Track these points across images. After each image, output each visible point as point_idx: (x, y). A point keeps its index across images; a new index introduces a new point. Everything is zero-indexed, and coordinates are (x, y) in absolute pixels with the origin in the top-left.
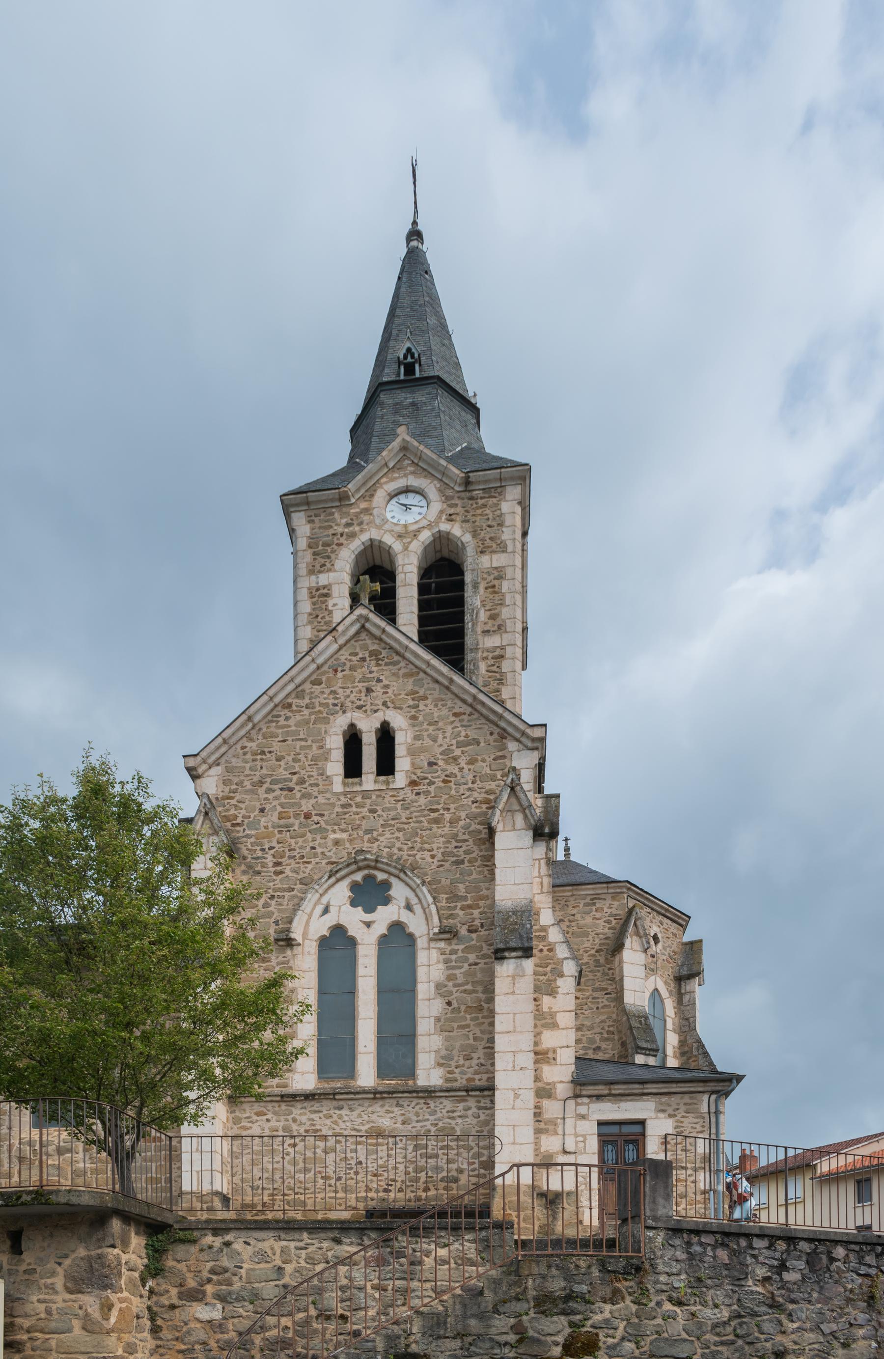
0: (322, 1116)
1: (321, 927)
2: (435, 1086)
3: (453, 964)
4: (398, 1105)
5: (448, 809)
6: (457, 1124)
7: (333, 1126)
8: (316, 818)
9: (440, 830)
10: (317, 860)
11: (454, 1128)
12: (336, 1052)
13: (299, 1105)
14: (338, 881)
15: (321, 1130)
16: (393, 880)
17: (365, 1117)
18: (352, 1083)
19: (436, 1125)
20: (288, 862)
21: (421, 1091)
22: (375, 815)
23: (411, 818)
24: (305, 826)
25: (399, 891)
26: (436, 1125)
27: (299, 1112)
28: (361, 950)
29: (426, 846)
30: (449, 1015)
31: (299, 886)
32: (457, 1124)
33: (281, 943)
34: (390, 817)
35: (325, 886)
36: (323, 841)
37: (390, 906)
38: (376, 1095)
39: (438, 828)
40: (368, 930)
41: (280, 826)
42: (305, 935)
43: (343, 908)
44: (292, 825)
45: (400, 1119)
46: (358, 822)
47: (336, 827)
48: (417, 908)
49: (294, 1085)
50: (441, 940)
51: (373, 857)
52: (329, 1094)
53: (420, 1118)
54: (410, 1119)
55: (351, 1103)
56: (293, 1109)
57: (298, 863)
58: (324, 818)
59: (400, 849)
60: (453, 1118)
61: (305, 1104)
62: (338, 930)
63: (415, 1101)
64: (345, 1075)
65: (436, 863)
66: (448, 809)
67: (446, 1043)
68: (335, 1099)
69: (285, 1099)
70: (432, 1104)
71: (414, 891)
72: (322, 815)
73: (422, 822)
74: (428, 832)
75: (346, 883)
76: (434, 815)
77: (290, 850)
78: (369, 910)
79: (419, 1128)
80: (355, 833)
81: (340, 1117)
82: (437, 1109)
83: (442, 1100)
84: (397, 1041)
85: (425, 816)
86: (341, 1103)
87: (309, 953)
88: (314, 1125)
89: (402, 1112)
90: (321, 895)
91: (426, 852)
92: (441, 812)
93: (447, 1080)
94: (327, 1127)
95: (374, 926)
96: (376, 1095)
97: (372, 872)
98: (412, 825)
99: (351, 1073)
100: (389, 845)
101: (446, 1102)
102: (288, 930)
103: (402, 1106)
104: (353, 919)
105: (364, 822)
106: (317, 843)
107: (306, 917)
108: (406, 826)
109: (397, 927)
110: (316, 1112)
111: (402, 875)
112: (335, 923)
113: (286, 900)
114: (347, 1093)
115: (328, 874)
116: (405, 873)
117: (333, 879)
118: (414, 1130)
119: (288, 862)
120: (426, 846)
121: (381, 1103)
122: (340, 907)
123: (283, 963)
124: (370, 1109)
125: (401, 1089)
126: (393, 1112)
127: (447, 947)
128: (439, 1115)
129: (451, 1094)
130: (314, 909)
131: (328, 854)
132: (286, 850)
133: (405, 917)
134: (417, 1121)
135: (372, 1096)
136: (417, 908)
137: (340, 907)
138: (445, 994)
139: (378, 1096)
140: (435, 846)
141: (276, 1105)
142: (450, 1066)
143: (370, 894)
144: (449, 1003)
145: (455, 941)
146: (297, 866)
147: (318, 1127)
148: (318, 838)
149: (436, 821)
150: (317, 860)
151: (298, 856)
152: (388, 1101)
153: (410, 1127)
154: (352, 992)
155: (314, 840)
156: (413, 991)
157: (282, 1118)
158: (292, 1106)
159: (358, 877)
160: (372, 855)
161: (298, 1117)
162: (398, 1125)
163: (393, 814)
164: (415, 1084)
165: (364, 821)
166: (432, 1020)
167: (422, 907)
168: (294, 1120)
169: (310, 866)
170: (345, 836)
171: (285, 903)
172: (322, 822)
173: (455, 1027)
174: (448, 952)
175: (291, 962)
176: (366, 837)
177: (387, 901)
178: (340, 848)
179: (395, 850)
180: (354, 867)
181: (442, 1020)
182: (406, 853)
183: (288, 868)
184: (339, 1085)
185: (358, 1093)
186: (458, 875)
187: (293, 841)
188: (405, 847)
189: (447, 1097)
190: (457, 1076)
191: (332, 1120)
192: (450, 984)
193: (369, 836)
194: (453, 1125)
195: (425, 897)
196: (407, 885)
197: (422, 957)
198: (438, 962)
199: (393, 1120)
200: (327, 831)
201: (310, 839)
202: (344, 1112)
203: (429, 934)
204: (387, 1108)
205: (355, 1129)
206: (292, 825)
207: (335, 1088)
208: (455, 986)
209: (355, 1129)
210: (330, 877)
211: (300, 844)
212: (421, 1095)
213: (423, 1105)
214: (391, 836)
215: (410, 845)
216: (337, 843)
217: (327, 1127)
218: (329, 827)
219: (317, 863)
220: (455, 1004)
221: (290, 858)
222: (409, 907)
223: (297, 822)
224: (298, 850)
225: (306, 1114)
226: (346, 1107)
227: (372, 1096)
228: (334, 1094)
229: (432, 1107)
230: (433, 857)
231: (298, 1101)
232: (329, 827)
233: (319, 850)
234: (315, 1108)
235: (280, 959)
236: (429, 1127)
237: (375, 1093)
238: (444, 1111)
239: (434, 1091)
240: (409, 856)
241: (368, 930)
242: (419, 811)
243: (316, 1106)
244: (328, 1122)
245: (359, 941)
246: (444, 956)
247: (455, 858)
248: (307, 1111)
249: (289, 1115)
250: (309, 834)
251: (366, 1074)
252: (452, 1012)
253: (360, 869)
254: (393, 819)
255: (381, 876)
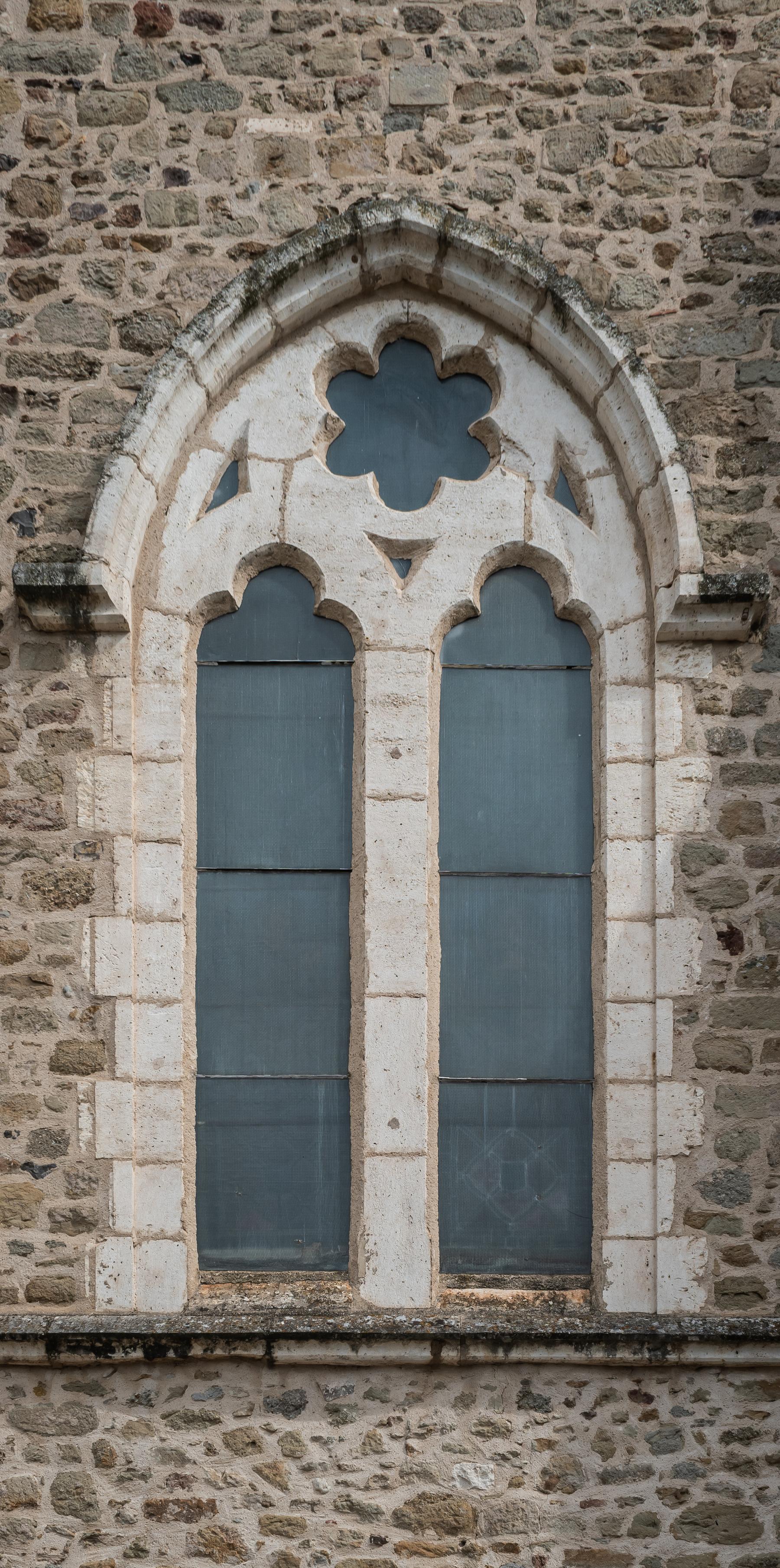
0: (218, 1443)
1: (208, 555)
2: (676, 1318)
3: (748, 757)
4: (528, 1400)
5: (729, 37)
6: (761, 1495)
7: (264, 1487)
8: (185, 35)
9: (693, 133)
10: (194, 235)
11: (748, 1513)
12: (275, 1163)
13: (122, 1387)
14: (285, 336)
15: (212, 1506)
16: (505, 357)
17: (395, 1452)
18: (340, 1292)
19: (680, 1496)
20: (73, 232)
21: (628, 1340)
22: (433, 40)
23: (578, 68)
24: (144, 69)
25: (527, 409)
26: (680, 1496)
27: (122, 1418)
28: (377, 674)
29: (639, 203)
30: (731, 992)
31: (115, 356)
32: (761, 1495)
33: (46, 614)
34: (493, 54)
35: (230, 353)
36: (216, 145)
37: (493, 475)
38: (442, 1353)
39: (688, 121)
40: (407, 576)
41: (34, 61)
42: (145, 583)
43: (303, 473)
44: (87, 62)
45: (537, 1463)
46: (362, 68)
47: (271, 85)
48: (603, 495)
49: (102, 1293)
50: (699, 642)
51: (430, 222)
52: (249, 1338)
53: (617, 1462)
54: (577, 1466)
55: (335, 1382)
56: (96, 1402)
57: (114, 243)
58: (225, 38)
59: (533, 212)
60: (746, 1467)
61: (149, 1384)
62: (282, 567)
63: (597, 1384)
64: (310, 1254)
65: (681, 289)
66: (729, 37)
67: (718, 1124)
68: (271, 1363)
69: (65, 1357)
70: (664, 1404)
71: (588, 408)
72: (213, 23)
73: (621, 88)
74: (646, 137)
75: (308, 359)
76: (671, 61)
77: (79, 179)
78: (407, 493)
79: (611, 1509)
80: (349, 117)
81: (292, 1447)
82: (685, 1422)
83: (706, 1382)
84: (526, 1130)
85: (633, 63)
86: (297, 1382)
87: (160, 672)
88: (183, 1482)
89: (545, 1432)
90: (213, 402)
91: (638, 234)
92: (700, 47)
93: (725, 1292)
94: (238, 1495)
95: (429, 565)
96: (442, 1353)
97: (418, 309)
98: (582, 98)
99: (336, 1247)
100: (488, 184)
101: (719, 1392)
102: (75, 556)
103: (543, 1405)
104: (339, 522)
105: (385, 70)
106: (190, 151)
107: (146, 503)
108: (557, 105)
109: (520, 566)
110: (191, 1420)
111: (545, 326)
112: (266, 540)
113: (63, 415)
114: (323, 1338)
115: (239, 289)
116: (561, 311)
117: (259, 326)
118: (592, 1514)
119: (73, 232)
120: (639, 203)
121: (457, 1387)
122: (288, 465)
123: (51, 716)
124: (414, 1416)
125: (544, 1325)
126: (505, 1432)
127: (721, 677)
128: (692, 1451)
129: (745, 1355)
130: (180, 465)
131: (237, 208)
132: (64, 179)
133: (551, 531)
134: (605, 1478)
135: (421, 1353)
136: (603, 495)
137: (288, 465)
138: (716, 895)
139: (449, 1354)
140: (674, 204)
141: (27, 1382)
142: (732, 1227)
143: (411, 412)
144: (731, 939)
145: (752, 654)
146: (111, 255)
147: (203, 1494)
148: (198, 136)
149: (681, 89)
150: (194, 235)
151: (112, 210)
152: (486, 1377)
153: (574, 1500)
154: (340, 873)
155: (178, 138)
156: (587, 879)
157: (51, 1445)
158: (94, 1390)
159: (362, 329)
160: (425, 206)
161: (116, 1443)
162: (527, 1493)
163: (504, 40)
164: (594, 1305)
165: (387, 65)
166: (665, 1011)
167: (623, 488)
168: (103, 1458)
169: (164, 263)
170: (306, 127)
171: (61, 432)
172: (212, 56)
173: (758, 1050)
174: (726, 702)
175: (88, 710)
176: (398, 142)
177: (478, 452)
178: (289, 183)
179: (513, 214)
180: (344, 272)
181: (704, 1014)
182: (556, 228)
183: (72, 263)
184: (285, 1299)
185: (370, 1337)
186: (766, 350)
187: (90, 136)
188: (553, 203)
189: (723, 1368)
190: (762, 1272)
191: (259, 1460)
192: (736, 850)
193: (409, 136)
194: (749, 1501)
195: (643, 426)
196: (563, 380)
197: (622, 721)
198: (688, 745)
199: (508, 1471)
200: (233, 97)
201: (164, 134)
202: (309, 1426)
203: (650, 615)
204: (482, 1411)
205: (353, 1508)
206: (87, 62)
207: (272, 1314)
208: (754, 859)
209: (353, 1508)
210: (249, 306)
211: (121, 151)
212: (624, 1355)
213: (625, 1405)
214: (497, 146)
215: (575, 194)
216: (275, 158)
217: (238, 1495)
218: (240, 83)
219: (193, 249)
220: (756, 947)
221: (79, 215)
222: (568, 490)
223: (106, 49)
224: (114, 183)
225: (149, 1429)
226: (314, 1400)
227: (421, 1353)
228: (271, 1339)
229: (665, 1416)
230: (666, 255)
231: (116, 1367)
232: (240, 83)
233: (201, 189)
234: (186, 1404)
235: (42, 693)
236: (653, 1504)
237: (438, 1341)
238: (712, 1434)
239: (680, 1341)
240: (572, 243)
241: (407, 576)
242: (607, 38)
243: (195, 1394)
244: (242, 1469)
245: (369, 632)
246: (709, 721)
247: (754, 269)
248: (155, 1418)
249: (79, 1431)
250: (157, 108)
251: (399, 1264)
252: (744, 981)
253: (369, 290)
254: (505, 67)
255: (456, 334)
